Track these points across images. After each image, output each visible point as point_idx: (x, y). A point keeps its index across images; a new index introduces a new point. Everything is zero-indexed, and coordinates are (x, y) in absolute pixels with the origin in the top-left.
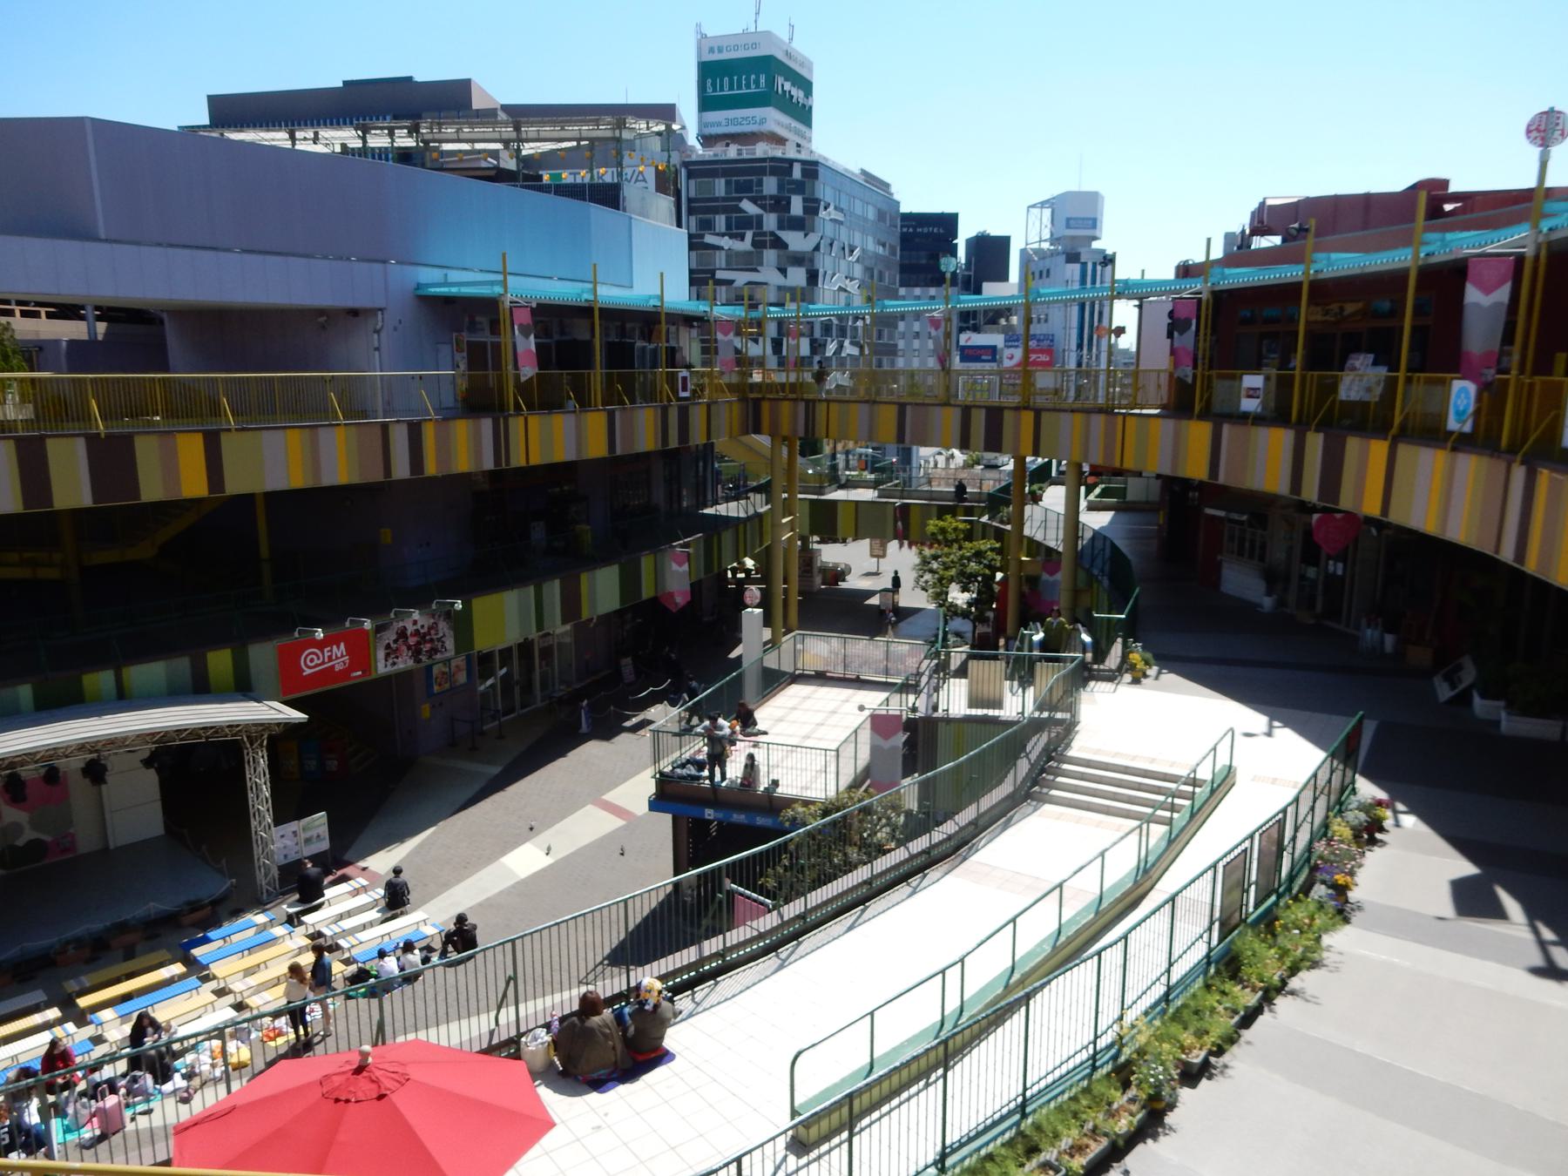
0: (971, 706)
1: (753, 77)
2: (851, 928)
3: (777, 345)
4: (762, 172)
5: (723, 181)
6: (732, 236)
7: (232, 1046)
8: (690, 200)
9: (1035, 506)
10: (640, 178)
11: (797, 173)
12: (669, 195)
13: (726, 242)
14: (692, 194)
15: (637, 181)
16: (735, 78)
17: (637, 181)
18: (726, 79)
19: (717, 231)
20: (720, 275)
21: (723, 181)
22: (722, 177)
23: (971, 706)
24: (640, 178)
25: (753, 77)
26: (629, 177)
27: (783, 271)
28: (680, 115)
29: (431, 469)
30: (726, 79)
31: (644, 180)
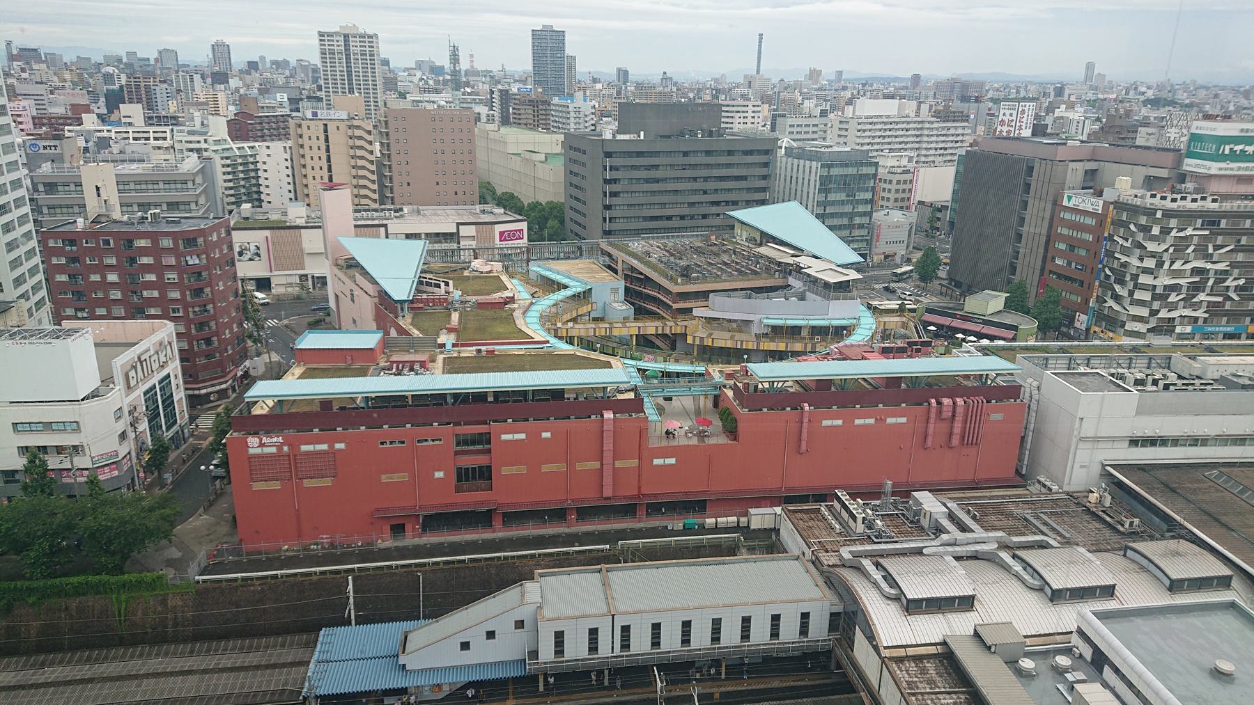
3: (1131, 293)
6: (1123, 238)
13: (1121, 241)
20: (1116, 255)
27: (1141, 260)
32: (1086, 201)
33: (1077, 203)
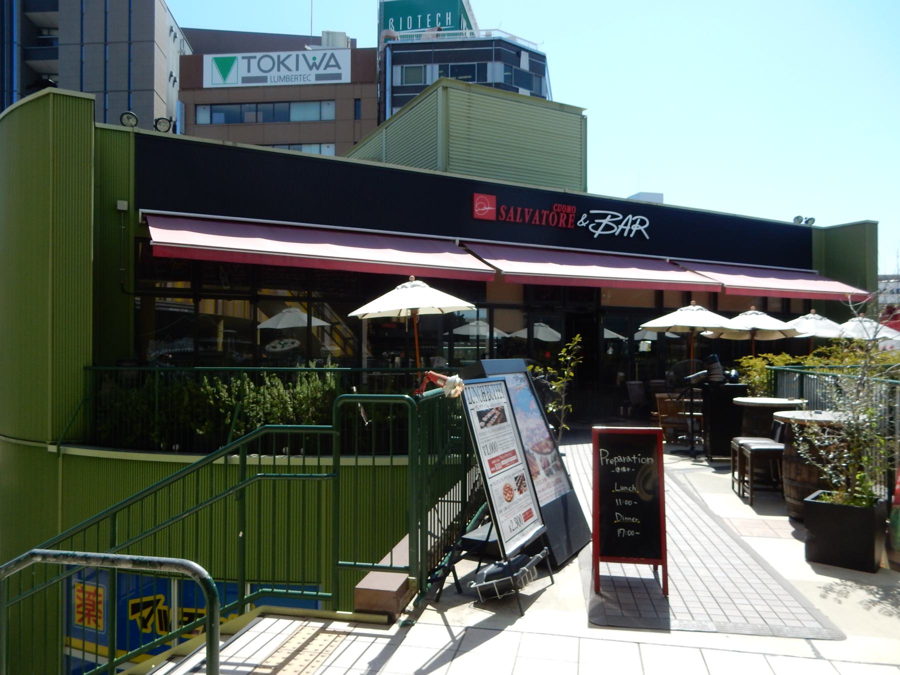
0: (243, 83)
1: (438, 15)
2: (366, 314)
4: (487, 56)
5: (436, 67)
7: (95, 599)
8: (394, 89)
9: (60, 41)
10: (332, 62)
11: (525, 63)
12: (383, 25)
14: (397, 82)
15: (327, 66)
16: (419, 16)
17: (327, 66)
18: (410, 18)
19: (489, 80)
21: (436, 67)
22: (435, 62)
23: (243, 83)
24: (332, 62)
25: (438, 15)
26: (318, 62)
28: (151, 658)
29: (193, 308)
30: (410, 18)
31: (337, 65)
32: (291, 63)
33: (255, 72)
